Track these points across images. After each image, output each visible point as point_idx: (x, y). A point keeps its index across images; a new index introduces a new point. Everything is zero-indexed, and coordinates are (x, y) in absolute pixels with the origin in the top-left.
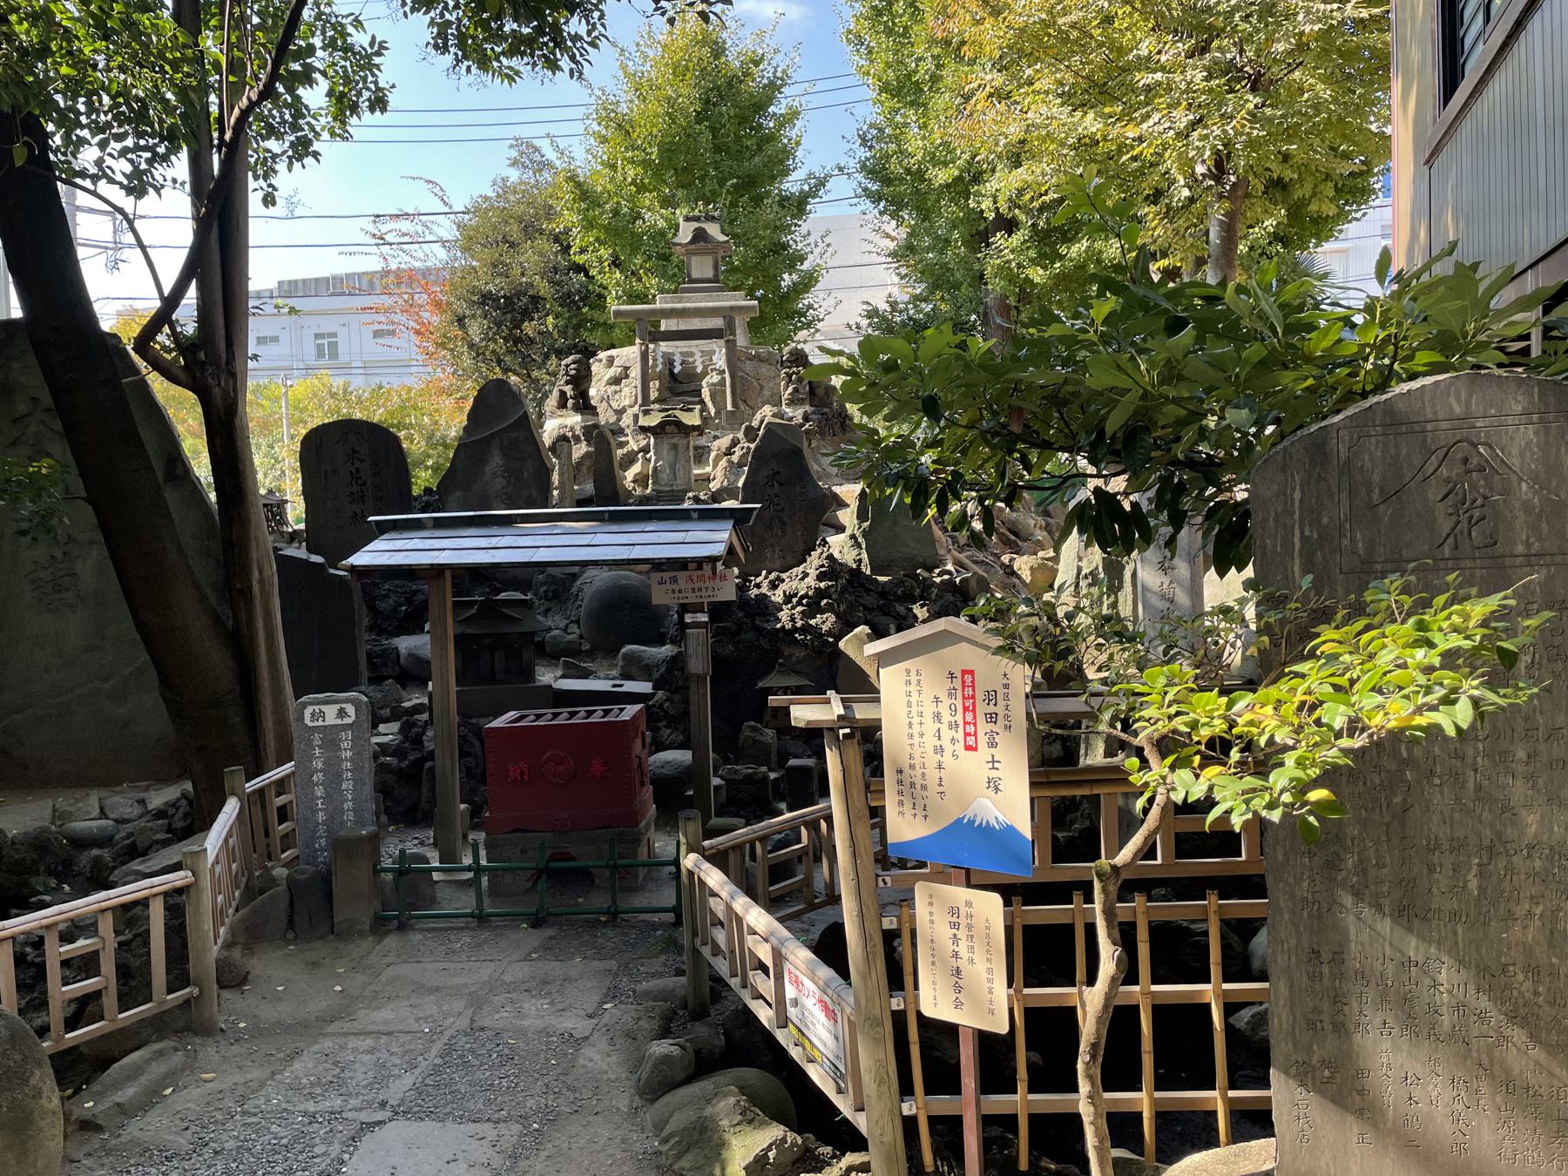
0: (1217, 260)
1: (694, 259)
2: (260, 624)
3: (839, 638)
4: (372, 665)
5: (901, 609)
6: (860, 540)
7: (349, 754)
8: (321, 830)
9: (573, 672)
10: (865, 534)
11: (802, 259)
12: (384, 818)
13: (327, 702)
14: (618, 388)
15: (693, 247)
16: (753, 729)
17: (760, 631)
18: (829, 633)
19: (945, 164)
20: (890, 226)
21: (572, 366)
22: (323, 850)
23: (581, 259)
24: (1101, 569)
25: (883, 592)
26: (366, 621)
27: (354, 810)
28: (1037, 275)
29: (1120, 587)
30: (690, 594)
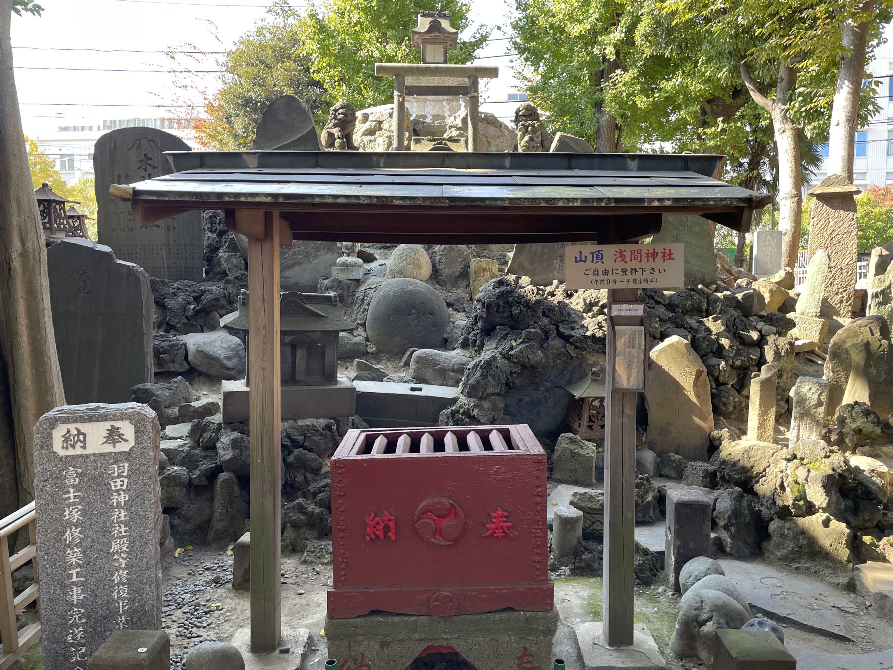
1: (429, 47)
2: (21, 307)
4: (159, 361)
5: (692, 322)
7: (123, 498)
8: (77, 615)
9: (366, 373)
12: (170, 542)
13: (91, 419)
14: (372, 138)
15: (428, 36)
17: (566, 339)
19: (580, 22)
21: (341, 111)
22: (78, 644)
23: (316, 77)
26: (154, 317)
27: (129, 583)
28: (642, 102)
30: (619, 277)
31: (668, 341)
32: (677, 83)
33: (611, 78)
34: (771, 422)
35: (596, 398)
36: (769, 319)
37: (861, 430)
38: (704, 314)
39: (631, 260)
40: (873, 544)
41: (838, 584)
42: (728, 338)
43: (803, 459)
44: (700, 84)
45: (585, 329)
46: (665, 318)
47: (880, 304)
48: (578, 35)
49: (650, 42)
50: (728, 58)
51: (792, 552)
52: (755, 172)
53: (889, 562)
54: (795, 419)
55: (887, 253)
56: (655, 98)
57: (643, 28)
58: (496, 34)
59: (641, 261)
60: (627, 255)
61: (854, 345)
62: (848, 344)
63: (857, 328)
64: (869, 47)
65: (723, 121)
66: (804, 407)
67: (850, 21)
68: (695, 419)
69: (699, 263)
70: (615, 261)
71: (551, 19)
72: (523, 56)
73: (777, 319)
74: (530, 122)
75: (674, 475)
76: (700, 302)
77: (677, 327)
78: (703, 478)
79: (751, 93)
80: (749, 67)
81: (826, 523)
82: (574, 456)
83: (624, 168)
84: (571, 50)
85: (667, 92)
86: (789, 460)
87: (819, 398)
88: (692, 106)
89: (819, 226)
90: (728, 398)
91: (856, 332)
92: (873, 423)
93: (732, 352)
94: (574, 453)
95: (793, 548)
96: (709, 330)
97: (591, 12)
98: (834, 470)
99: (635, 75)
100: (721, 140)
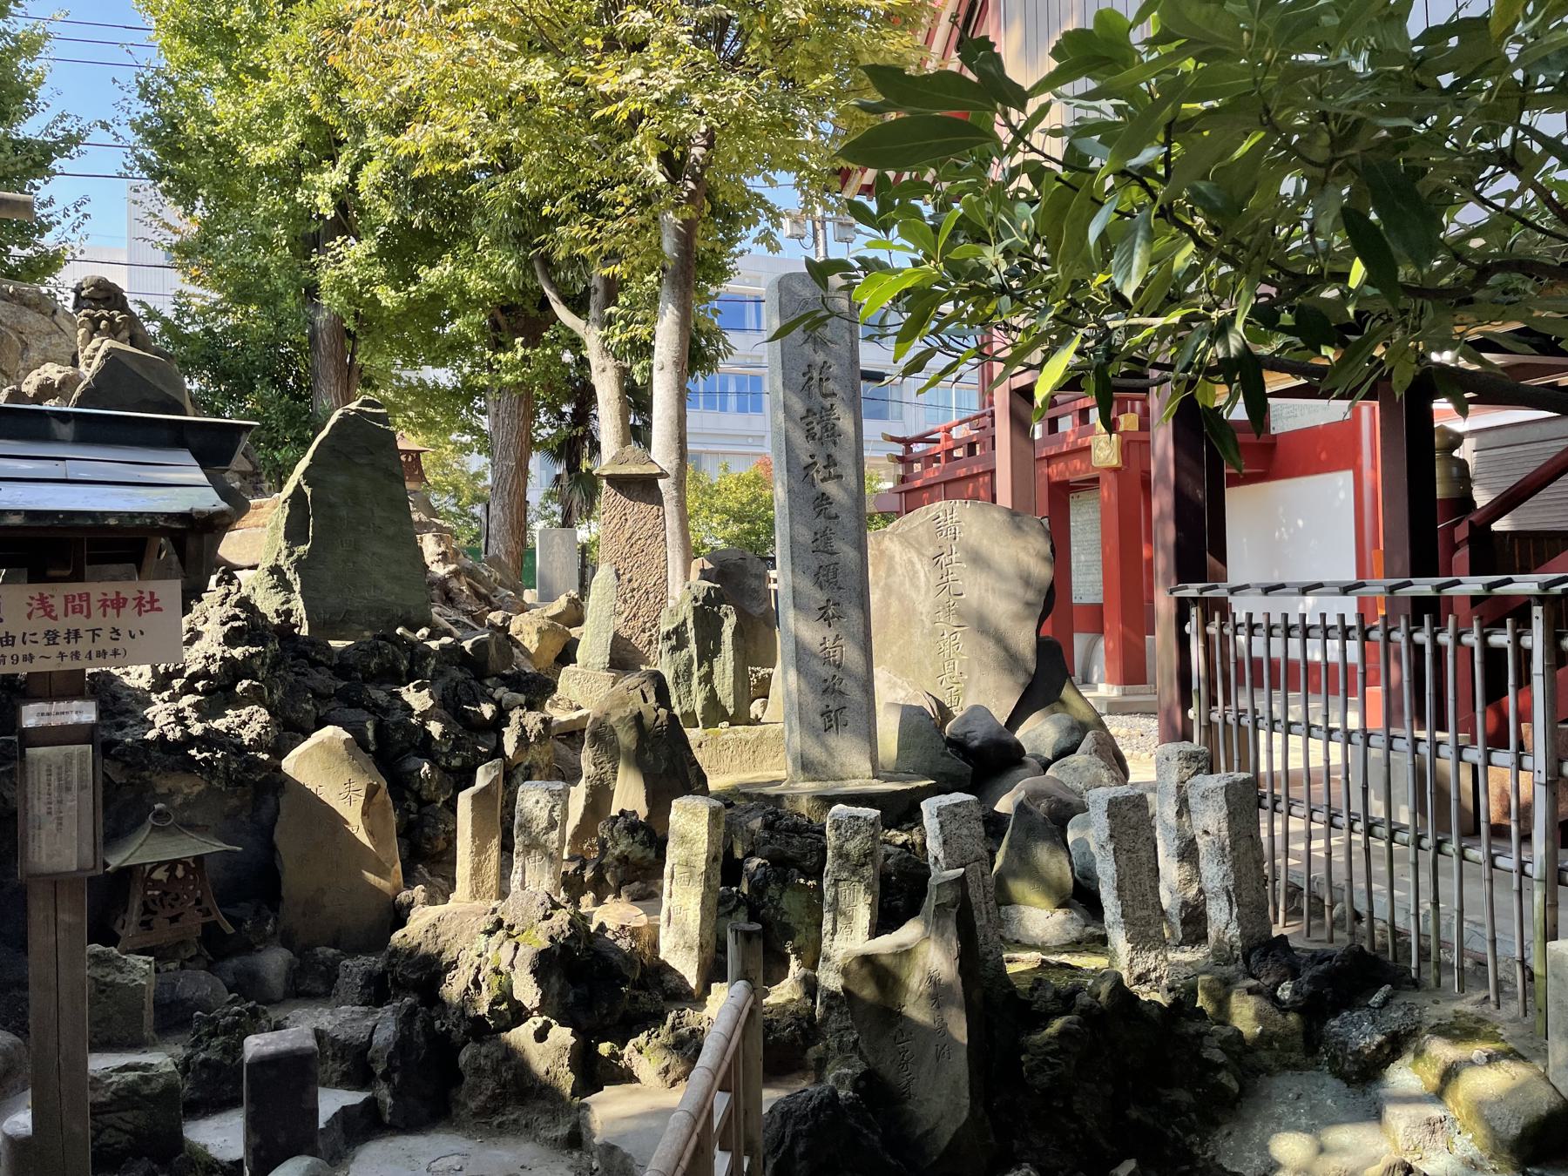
0: (675, 276)
3: (280, 751)
5: (380, 695)
6: (290, 576)
10: (300, 566)
11: (44, 228)
16: (98, 959)
18: (258, 744)
19: (266, 142)
20: (172, 212)
24: (690, 624)
25: (342, 666)
28: (387, 297)
29: (717, 651)
30: (40, 649)
31: (318, 736)
32: (446, 273)
33: (329, 249)
34: (492, 863)
35: (160, 864)
36: (516, 682)
37: (626, 857)
38: (404, 680)
39: (66, 615)
40: (613, 1055)
41: (556, 1140)
42: (440, 720)
43: (511, 927)
44: (483, 279)
45: (147, 726)
46: (326, 691)
47: (673, 649)
48: (262, 163)
49: (386, 197)
50: (514, 244)
51: (493, 1097)
52: (580, 428)
53: (638, 1080)
54: (518, 855)
55: (711, 566)
56: (410, 293)
57: (371, 174)
58: (98, 135)
59: (88, 616)
60: (58, 603)
61: (621, 719)
62: (613, 720)
63: (625, 692)
64: (730, 255)
65: (525, 345)
66: (530, 833)
67: (671, 215)
68: (367, 874)
69: (397, 589)
70: (29, 616)
71: (208, 127)
72: (159, 185)
73: (527, 681)
74: (105, 312)
75: (322, 989)
76: (396, 658)
77: (350, 707)
78: (362, 987)
79: (554, 305)
80: (546, 260)
81: (541, 1035)
82: (104, 991)
83: (47, 437)
84: (253, 188)
85: (430, 286)
86: (490, 933)
87: (550, 816)
88: (473, 313)
89: (612, 525)
90: (435, 827)
91: (622, 698)
92: (643, 843)
93: (446, 745)
94: (105, 984)
95: (493, 1090)
96: (408, 708)
97: (286, 128)
98: (552, 939)
99: (373, 250)
100: (523, 374)
